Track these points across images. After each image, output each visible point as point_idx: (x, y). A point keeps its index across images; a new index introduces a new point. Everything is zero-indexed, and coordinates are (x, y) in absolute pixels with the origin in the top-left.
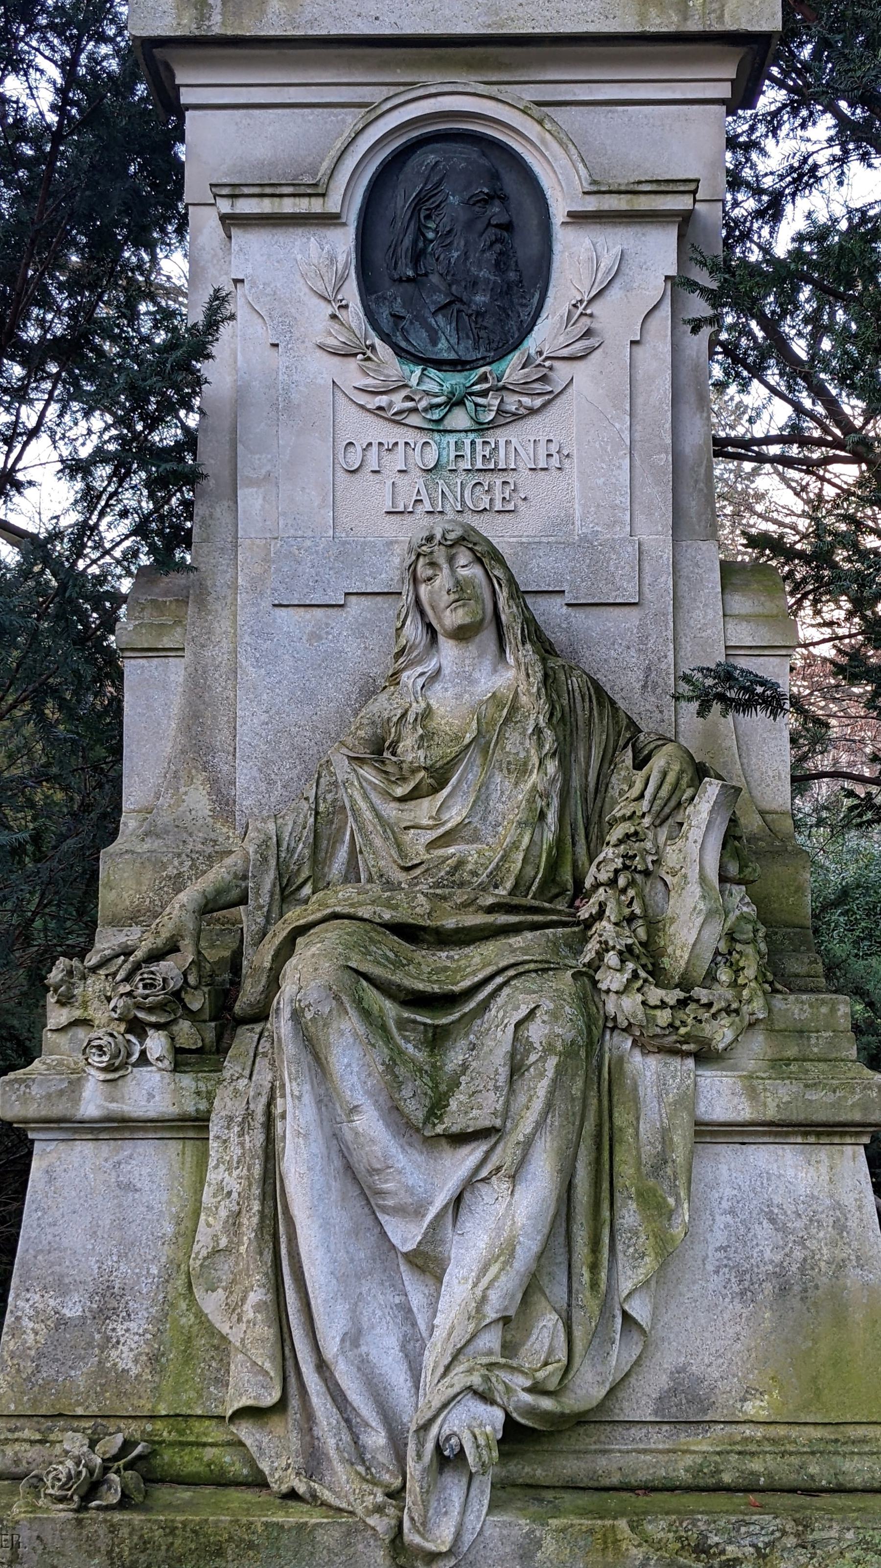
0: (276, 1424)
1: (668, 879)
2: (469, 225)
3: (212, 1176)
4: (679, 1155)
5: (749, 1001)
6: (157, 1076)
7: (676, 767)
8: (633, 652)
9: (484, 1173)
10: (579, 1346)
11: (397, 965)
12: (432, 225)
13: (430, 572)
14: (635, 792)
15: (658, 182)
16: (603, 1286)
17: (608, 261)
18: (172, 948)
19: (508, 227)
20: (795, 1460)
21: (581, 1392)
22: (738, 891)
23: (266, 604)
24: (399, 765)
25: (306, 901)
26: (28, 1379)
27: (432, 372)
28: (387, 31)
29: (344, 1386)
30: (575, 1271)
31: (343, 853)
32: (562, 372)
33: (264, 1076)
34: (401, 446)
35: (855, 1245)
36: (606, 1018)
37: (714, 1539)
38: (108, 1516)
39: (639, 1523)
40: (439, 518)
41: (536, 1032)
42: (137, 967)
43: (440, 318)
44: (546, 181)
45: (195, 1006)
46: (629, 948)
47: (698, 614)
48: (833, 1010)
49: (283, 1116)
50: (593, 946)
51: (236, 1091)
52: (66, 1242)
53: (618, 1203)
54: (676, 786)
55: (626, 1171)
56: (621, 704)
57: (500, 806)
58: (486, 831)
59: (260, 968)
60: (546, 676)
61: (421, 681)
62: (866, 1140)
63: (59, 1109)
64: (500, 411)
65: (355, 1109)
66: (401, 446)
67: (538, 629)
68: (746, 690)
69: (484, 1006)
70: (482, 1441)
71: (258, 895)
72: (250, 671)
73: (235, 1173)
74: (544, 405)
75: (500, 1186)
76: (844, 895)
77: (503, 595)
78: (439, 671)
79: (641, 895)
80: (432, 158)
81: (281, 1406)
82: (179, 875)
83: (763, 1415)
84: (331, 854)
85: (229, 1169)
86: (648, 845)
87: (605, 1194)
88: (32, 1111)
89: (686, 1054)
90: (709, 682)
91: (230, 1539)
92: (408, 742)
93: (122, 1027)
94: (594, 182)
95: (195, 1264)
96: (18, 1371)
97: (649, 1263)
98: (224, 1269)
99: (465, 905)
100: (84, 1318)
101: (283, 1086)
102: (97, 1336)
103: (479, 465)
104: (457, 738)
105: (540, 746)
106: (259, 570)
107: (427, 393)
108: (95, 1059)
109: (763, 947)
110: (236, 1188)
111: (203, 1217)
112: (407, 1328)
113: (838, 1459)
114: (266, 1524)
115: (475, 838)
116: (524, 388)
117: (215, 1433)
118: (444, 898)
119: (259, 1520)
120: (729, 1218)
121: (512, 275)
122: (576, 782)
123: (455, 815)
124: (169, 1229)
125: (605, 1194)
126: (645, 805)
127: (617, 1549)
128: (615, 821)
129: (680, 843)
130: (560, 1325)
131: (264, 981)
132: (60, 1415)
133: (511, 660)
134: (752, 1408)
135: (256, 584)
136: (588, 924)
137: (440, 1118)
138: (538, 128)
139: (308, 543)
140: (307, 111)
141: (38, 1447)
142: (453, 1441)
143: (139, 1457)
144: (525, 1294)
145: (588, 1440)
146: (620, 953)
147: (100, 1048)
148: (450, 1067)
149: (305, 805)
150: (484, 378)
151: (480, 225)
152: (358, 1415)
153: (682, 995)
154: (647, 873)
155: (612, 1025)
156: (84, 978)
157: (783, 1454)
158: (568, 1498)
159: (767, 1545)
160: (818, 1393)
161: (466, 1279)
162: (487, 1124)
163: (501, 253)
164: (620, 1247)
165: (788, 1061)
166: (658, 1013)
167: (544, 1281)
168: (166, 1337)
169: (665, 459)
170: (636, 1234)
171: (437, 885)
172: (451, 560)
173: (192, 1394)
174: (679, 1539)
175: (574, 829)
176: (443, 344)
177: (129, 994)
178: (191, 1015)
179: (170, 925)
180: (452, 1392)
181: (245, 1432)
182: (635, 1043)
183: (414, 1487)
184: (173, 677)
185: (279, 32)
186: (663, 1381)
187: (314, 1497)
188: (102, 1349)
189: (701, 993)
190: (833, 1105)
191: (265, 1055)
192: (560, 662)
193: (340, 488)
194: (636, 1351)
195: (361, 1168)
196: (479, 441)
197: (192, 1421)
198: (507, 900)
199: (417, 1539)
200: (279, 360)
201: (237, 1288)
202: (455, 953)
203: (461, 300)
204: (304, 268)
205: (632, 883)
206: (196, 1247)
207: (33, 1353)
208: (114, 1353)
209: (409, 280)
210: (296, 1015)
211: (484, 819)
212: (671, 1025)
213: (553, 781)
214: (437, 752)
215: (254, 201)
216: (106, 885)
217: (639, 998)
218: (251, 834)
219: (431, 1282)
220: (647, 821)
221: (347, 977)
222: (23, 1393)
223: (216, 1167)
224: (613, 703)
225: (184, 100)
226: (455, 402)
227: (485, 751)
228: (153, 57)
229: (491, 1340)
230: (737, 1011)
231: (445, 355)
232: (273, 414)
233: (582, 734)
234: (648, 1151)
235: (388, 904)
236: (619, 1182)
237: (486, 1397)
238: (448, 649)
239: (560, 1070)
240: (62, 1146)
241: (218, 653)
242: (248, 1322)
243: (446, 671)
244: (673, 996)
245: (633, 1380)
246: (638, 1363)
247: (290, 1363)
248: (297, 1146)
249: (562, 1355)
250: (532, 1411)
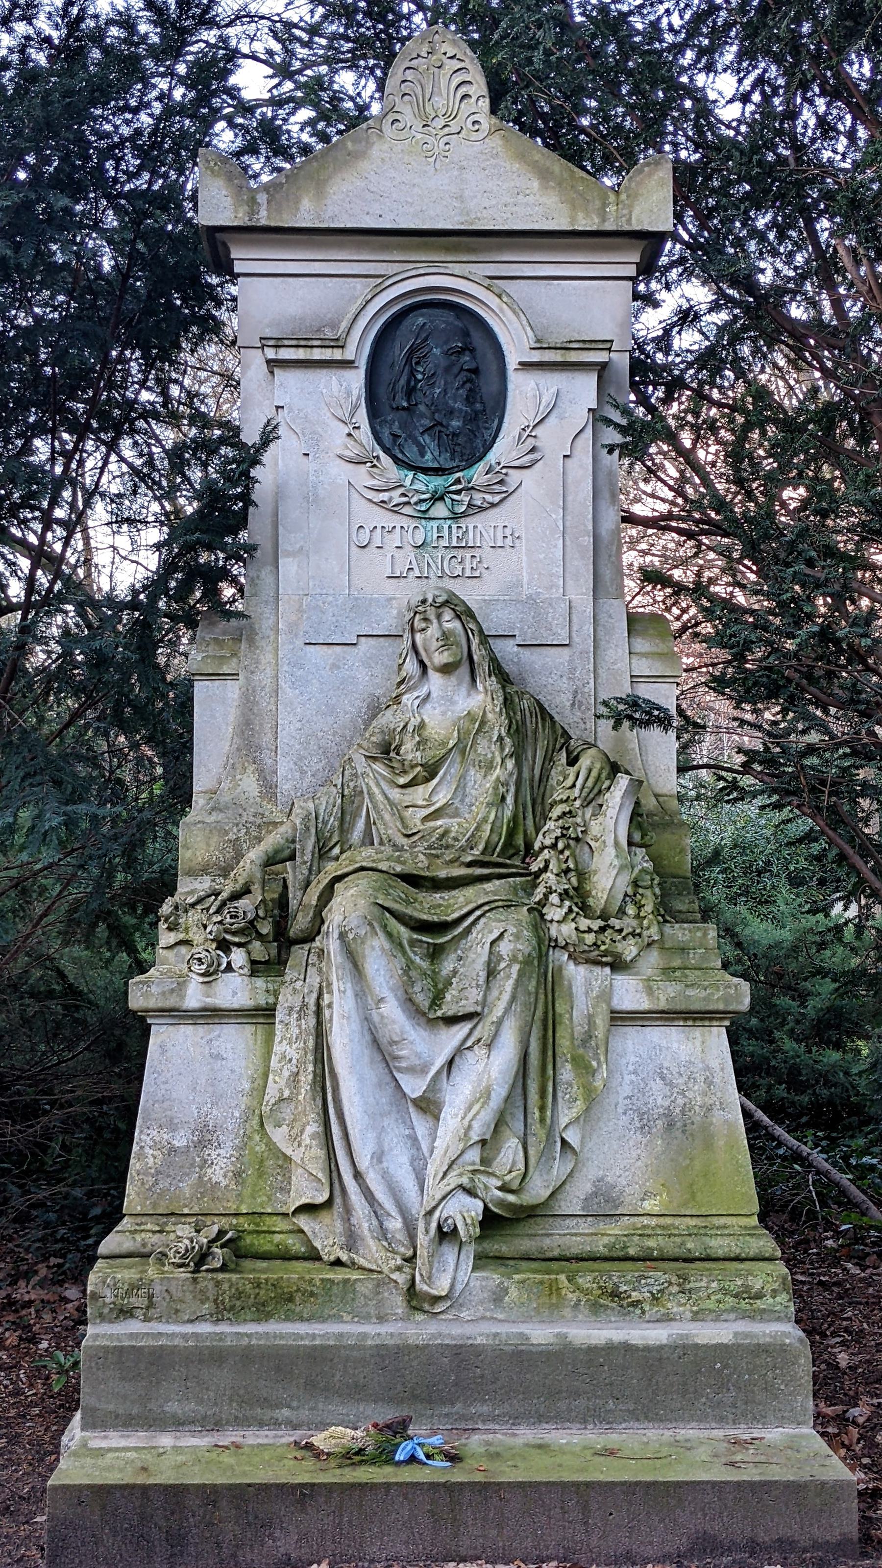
0: (325, 1217)
1: (592, 843)
2: (447, 370)
3: (277, 1048)
4: (600, 1033)
5: (648, 928)
6: (239, 979)
7: (598, 766)
8: (564, 680)
9: (469, 1043)
10: (532, 1161)
11: (408, 903)
12: (420, 369)
13: (424, 625)
14: (569, 782)
15: (584, 341)
16: (548, 1121)
17: (547, 398)
18: (246, 891)
19: (476, 371)
20: (678, 1240)
21: (534, 1192)
22: (641, 852)
23: (299, 643)
24: (402, 762)
25: (337, 859)
26: (150, 1189)
27: (421, 476)
28: (388, 226)
29: (373, 1188)
30: (529, 1110)
31: (361, 824)
32: (515, 477)
33: (314, 979)
34: (398, 529)
35: (719, 1094)
36: (550, 940)
37: (623, 1288)
38: (215, 1275)
39: (574, 1278)
40: (425, 581)
41: (505, 948)
42: (224, 904)
43: (426, 437)
44: (503, 338)
45: (264, 931)
46: (566, 891)
47: (611, 652)
48: (705, 934)
49: (330, 1006)
50: (540, 891)
51: (294, 989)
52: (174, 1095)
53: (559, 1065)
54: (598, 779)
55: (564, 1043)
56: (557, 718)
57: (474, 792)
58: (464, 809)
59: (309, 905)
60: (505, 699)
61: (417, 702)
62: (727, 1023)
63: (170, 1002)
64: (470, 505)
65: (381, 1000)
66: (398, 529)
67: (499, 665)
68: (647, 713)
69: (468, 931)
70: (469, 1221)
71: (303, 854)
72: (287, 691)
74: (502, 501)
75: (480, 1052)
76: (716, 856)
77: (475, 642)
78: (429, 695)
79: (573, 855)
80: (421, 320)
81: (329, 1203)
82: (237, 839)
83: (656, 1210)
84: (353, 824)
85: (290, 1044)
86: (579, 820)
87: (550, 1059)
88: (152, 1004)
89: (604, 964)
90: (621, 707)
91: (298, 1290)
92: (408, 746)
93: (214, 946)
95: (266, 1109)
97: (580, 1105)
98: (287, 1112)
99: (452, 862)
100: (188, 1147)
101: (329, 985)
103: (454, 544)
104: (443, 744)
105: (502, 749)
106: (294, 618)
107: (417, 491)
108: (196, 967)
109: (657, 891)
110: (295, 1056)
111: (271, 1077)
112: (414, 1151)
113: (707, 1239)
114: (322, 1280)
115: (456, 814)
116: (487, 489)
117: (281, 1225)
118: (437, 857)
119: (317, 1277)
120: (633, 1077)
121: (478, 406)
122: (526, 774)
123: (441, 799)
124: (247, 1086)
125: (550, 1059)
126: (576, 792)
127: (559, 1295)
128: (555, 803)
129: (600, 819)
130: (520, 1146)
131: (311, 914)
132: (173, 1214)
133: (480, 687)
134: (649, 1205)
135: (293, 628)
136: (537, 875)
137: (440, 1006)
138: (497, 300)
139: (331, 598)
141: (158, 1235)
142: (450, 1221)
143: (230, 1240)
144: (496, 1126)
145: (537, 1227)
146: (560, 895)
147: (199, 960)
148: (444, 973)
149: (334, 790)
150: (458, 481)
151: (456, 370)
152: (382, 1208)
153: (602, 923)
154: (577, 840)
155: (555, 944)
156: (186, 911)
157: (670, 1236)
158: (524, 1264)
159: (659, 1291)
160: (693, 1196)
161: (456, 1115)
162: (472, 1010)
163: (470, 390)
164: (560, 1094)
165: (674, 970)
166: (586, 935)
167: (508, 1118)
168: (245, 1159)
169: (588, 541)
170: (571, 1085)
171: (430, 847)
172: (439, 616)
173: (265, 1198)
174: (600, 1288)
175: (525, 808)
176: (428, 456)
177: (220, 922)
178: (260, 937)
179: (245, 875)
180: (449, 1188)
181: (303, 1222)
182: (570, 956)
183: (423, 1253)
186: (588, 1188)
187: (354, 1263)
188: (201, 1168)
189: (616, 923)
190: (704, 999)
191: (313, 965)
192: (515, 689)
193: (353, 559)
194: (570, 1166)
195: (384, 1041)
196: (454, 526)
197: (264, 1217)
198: (481, 858)
199: (425, 1288)
200: (310, 465)
201: (298, 1125)
202: (446, 895)
203: (441, 424)
204: (328, 399)
205: (567, 847)
206: (266, 1098)
208: (209, 1171)
209: (404, 409)
210: (342, 936)
211: (462, 801)
212: (595, 944)
213: (511, 774)
214: (429, 753)
215: (292, 350)
216: (184, 846)
217: (573, 925)
218: (296, 810)
219: (430, 1119)
220: (577, 803)
221: (377, 910)
224: (552, 718)
225: (237, 270)
226: (437, 498)
227: (463, 752)
228: (214, 238)
229: (474, 1155)
230: (640, 935)
231: (430, 465)
232: (305, 504)
233: (530, 740)
234: (579, 1031)
235: (398, 860)
236: (558, 1051)
237: (470, 1192)
238: (435, 679)
239: (521, 974)
240: (171, 1028)
241: (264, 677)
243: (434, 695)
244: (596, 924)
245: (567, 1187)
246: (570, 1175)
247: (335, 1174)
248: (342, 1025)
249: (521, 1166)
250: (501, 1203)
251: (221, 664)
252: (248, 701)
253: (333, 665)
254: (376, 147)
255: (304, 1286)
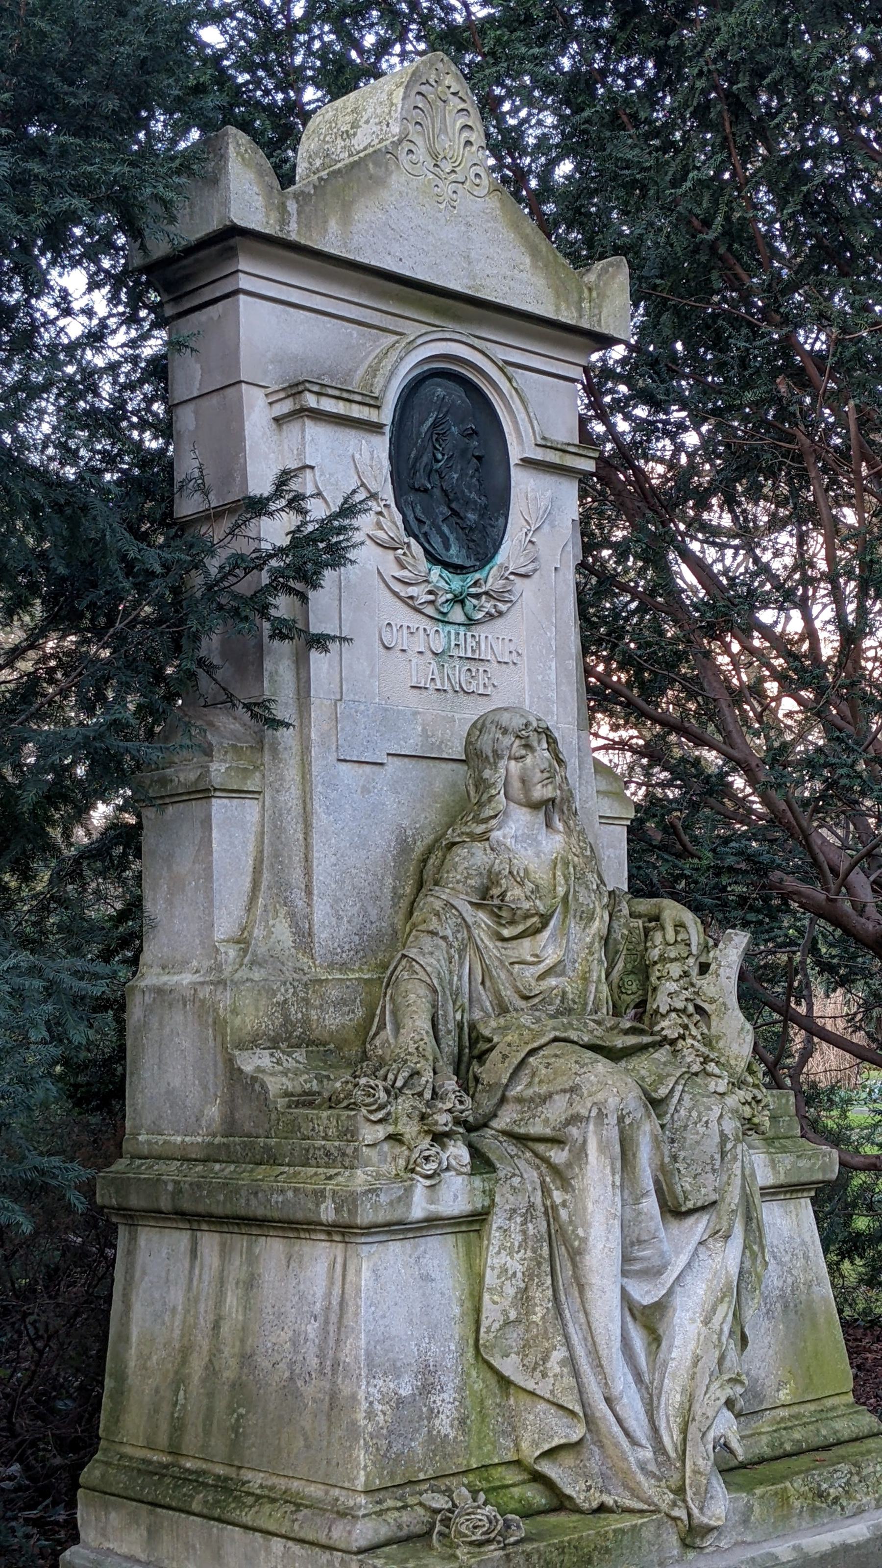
6: (460, 1179)
20: (811, 1427)
26: (385, 1456)
51: (513, 1188)
52: (393, 1332)
73: (517, 1257)
80: (440, 391)
83: (788, 1400)
94: (544, 438)
96: (378, 1449)
100: (413, 1395)
102: (424, 1409)
103: (469, 655)
110: (519, 1269)
111: (486, 1297)
114: (615, 1531)
115: (563, 974)
139: (362, 707)
140: (326, 319)
150: (476, 584)
168: (468, 1402)
173: (490, 1447)
184: (248, 818)
185: (336, 252)
188: (429, 1419)
207: (385, 1431)
208: (437, 1422)
210: (621, 1119)
215: (333, 401)
222: (383, 1468)
223: (498, 1253)
240: (381, 1247)
241: (291, 797)
242: (555, 1376)
251: (245, 778)
252: (276, 826)
253: (364, 786)
254: (394, 177)
255: (601, 1542)
